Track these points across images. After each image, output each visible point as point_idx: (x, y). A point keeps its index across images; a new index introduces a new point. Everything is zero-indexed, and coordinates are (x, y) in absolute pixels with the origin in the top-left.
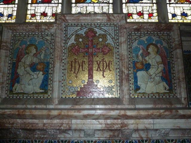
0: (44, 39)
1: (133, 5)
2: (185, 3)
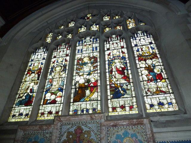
0: (44, 136)
1: (116, 100)
2: (160, 93)
